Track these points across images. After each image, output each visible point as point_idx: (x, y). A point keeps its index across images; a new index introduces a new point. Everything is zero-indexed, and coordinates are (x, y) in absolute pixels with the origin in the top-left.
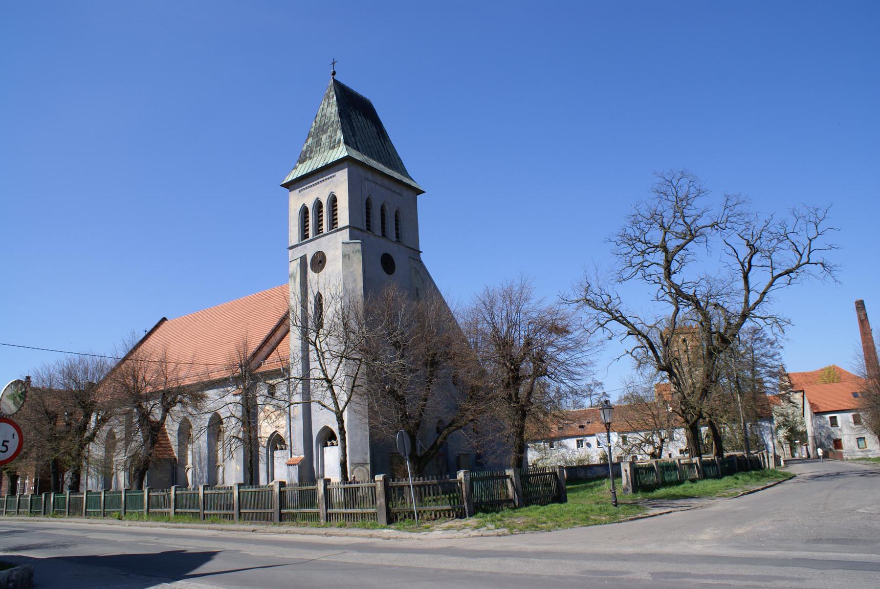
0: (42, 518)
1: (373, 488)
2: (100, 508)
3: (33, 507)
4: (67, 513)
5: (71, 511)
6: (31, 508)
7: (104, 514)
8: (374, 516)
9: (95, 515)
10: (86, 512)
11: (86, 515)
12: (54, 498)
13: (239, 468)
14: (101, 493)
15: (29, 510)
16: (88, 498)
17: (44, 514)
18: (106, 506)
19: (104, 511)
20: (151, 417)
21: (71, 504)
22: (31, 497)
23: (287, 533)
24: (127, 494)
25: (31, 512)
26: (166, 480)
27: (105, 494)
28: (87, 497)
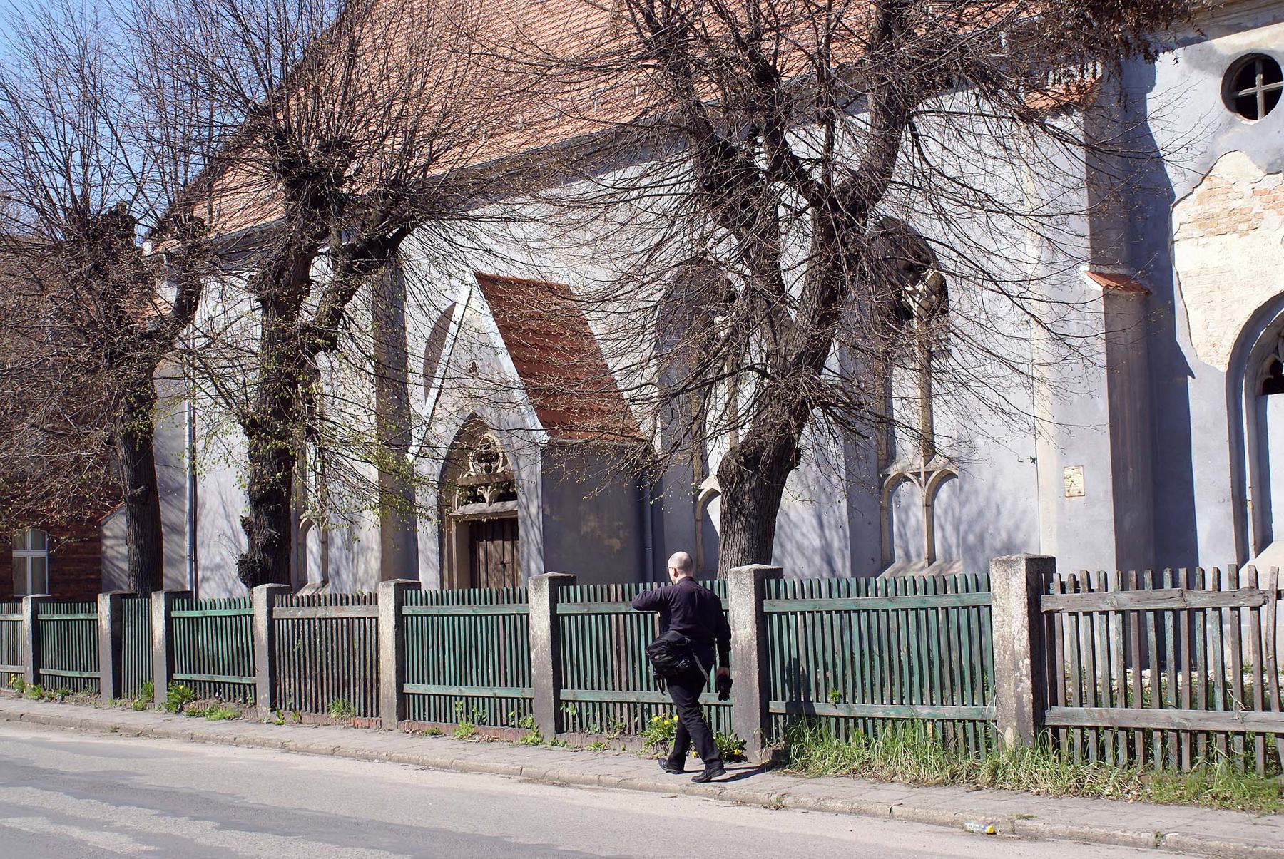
0: (107, 712)
1: (374, 620)
2: (523, 675)
3: (47, 656)
4: (264, 695)
5: (288, 686)
6: (38, 663)
7: (559, 716)
8: (524, 707)
9: (469, 718)
10: (402, 696)
11: (402, 717)
12: (169, 621)
13: (1079, 483)
14: (373, 599)
15: (28, 668)
16: (411, 625)
17: (117, 694)
18: (569, 675)
19: (558, 702)
20: (316, 258)
21: (282, 646)
22: (35, 613)
23: (115, 730)
24: (406, 610)
25: (38, 679)
26: (616, 543)
27: (554, 601)
28: (400, 619)
